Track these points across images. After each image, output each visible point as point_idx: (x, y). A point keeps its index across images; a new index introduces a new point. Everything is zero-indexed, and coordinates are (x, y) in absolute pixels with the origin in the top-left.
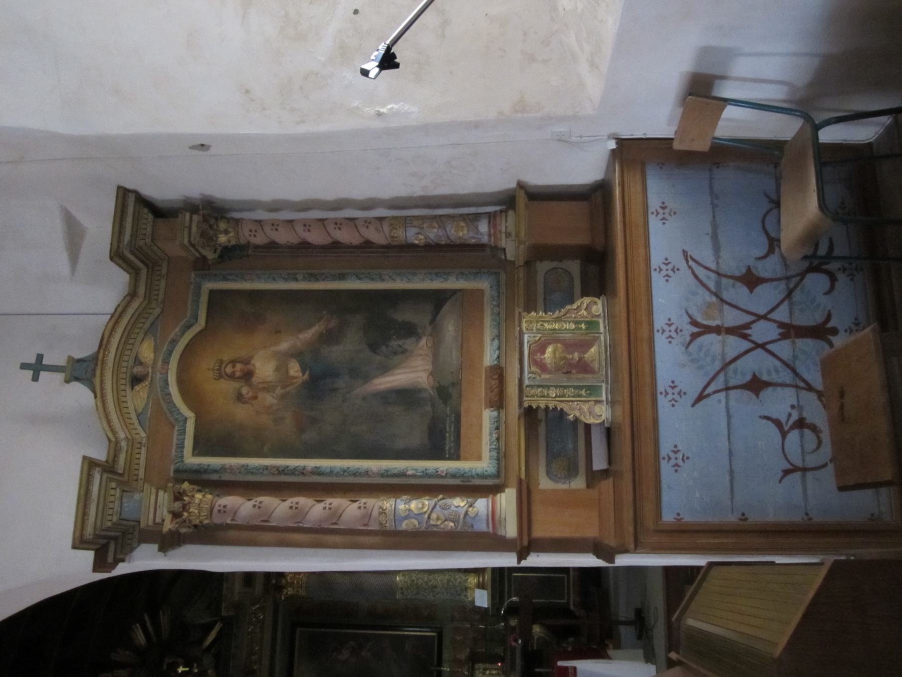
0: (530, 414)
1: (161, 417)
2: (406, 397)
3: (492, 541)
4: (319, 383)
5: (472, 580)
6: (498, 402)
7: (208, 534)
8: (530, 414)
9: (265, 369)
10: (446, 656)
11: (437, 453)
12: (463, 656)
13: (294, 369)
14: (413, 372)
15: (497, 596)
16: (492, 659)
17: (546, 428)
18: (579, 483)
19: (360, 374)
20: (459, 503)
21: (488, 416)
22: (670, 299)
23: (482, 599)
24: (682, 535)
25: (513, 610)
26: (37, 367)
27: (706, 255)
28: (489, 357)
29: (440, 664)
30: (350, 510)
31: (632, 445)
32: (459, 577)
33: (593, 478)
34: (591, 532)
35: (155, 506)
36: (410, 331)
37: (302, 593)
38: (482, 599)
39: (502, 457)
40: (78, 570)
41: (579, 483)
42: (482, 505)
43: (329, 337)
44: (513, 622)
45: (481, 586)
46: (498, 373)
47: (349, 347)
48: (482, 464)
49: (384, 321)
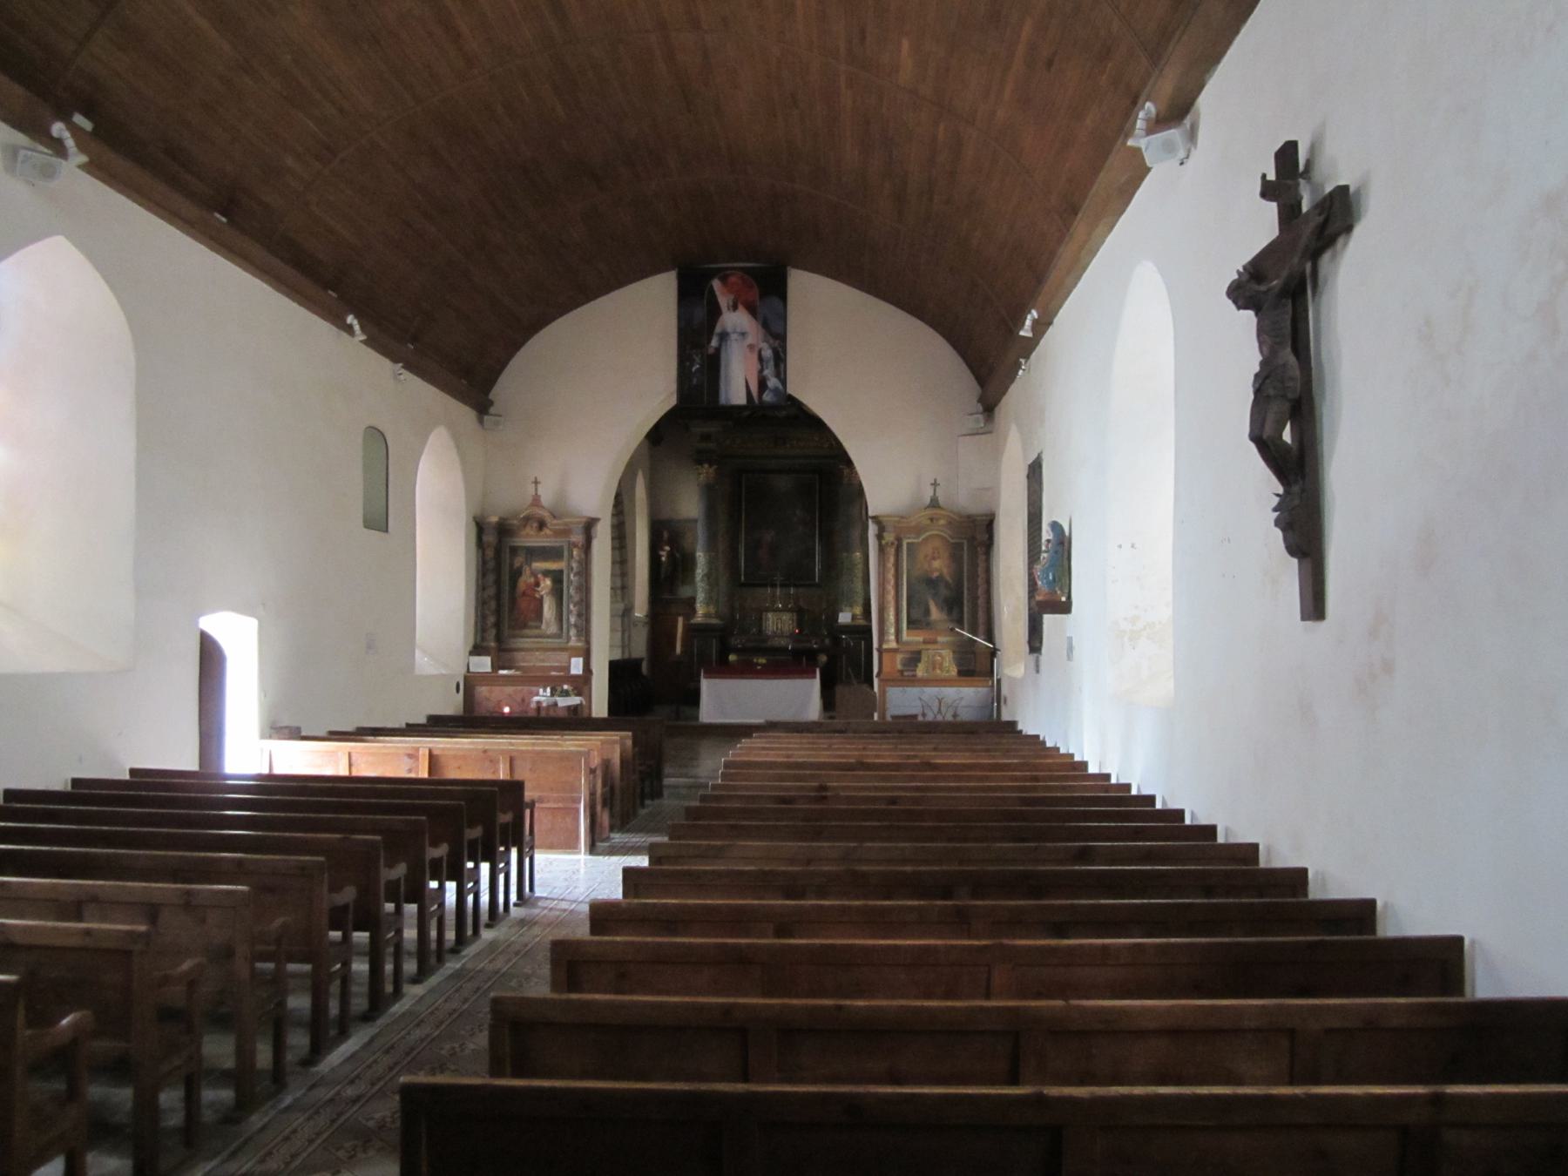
0: (919, 652)
1: (918, 530)
2: (927, 612)
3: (881, 641)
4: (931, 583)
5: (858, 610)
6: (925, 642)
7: (882, 550)
8: (919, 652)
9: (936, 564)
10: (801, 590)
11: (909, 622)
12: (801, 603)
13: (936, 574)
14: (936, 614)
15: (847, 629)
16: (800, 624)
17: (914, 659)
18: (899, 667)
19: (935, 596)
20: (892, 630)
21: (920, 639)
22: (950, 693)
23: (844, 618)
24: (883, 692)
25: (836, 640)
26: (935, 484)
27: (963, 703)
28: (940, 639)
29: (795, 586)
30: (891, 597)
31: (906, 678)
32: (860, 601)
33: (901, 672)
34: (885, 669)
35: (889, 537)
36: (950, 611)
37: (845, 481)
38: (844, 618)
39: (908, 643)
40: (871, 513)
41: (899, 667)
42: (893, 637)
43: (947, 584)
44: (827, 641)
45: (854, 617)
46: (934, 642)
47: (944, 592)
48: (905, 636)
49: (953, 605)
